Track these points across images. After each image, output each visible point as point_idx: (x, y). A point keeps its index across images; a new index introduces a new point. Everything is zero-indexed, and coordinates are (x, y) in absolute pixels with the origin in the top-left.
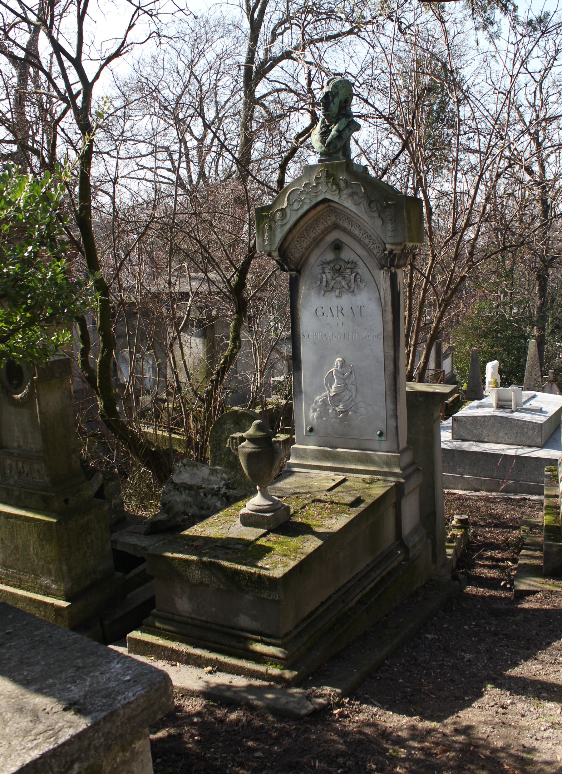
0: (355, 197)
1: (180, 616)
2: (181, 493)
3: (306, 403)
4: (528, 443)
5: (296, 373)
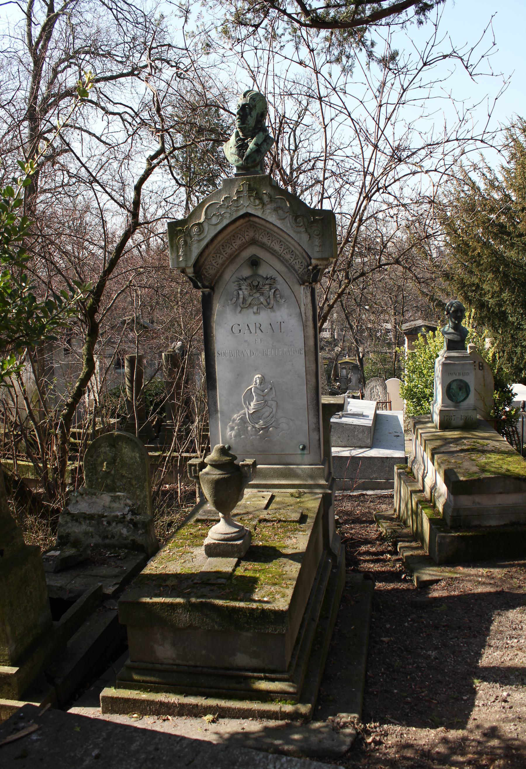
0: (280, 212)
1: (162, 664)
2: (80, 523)
3: (222, 422)
4: (358, 445)
5: (210, 392)
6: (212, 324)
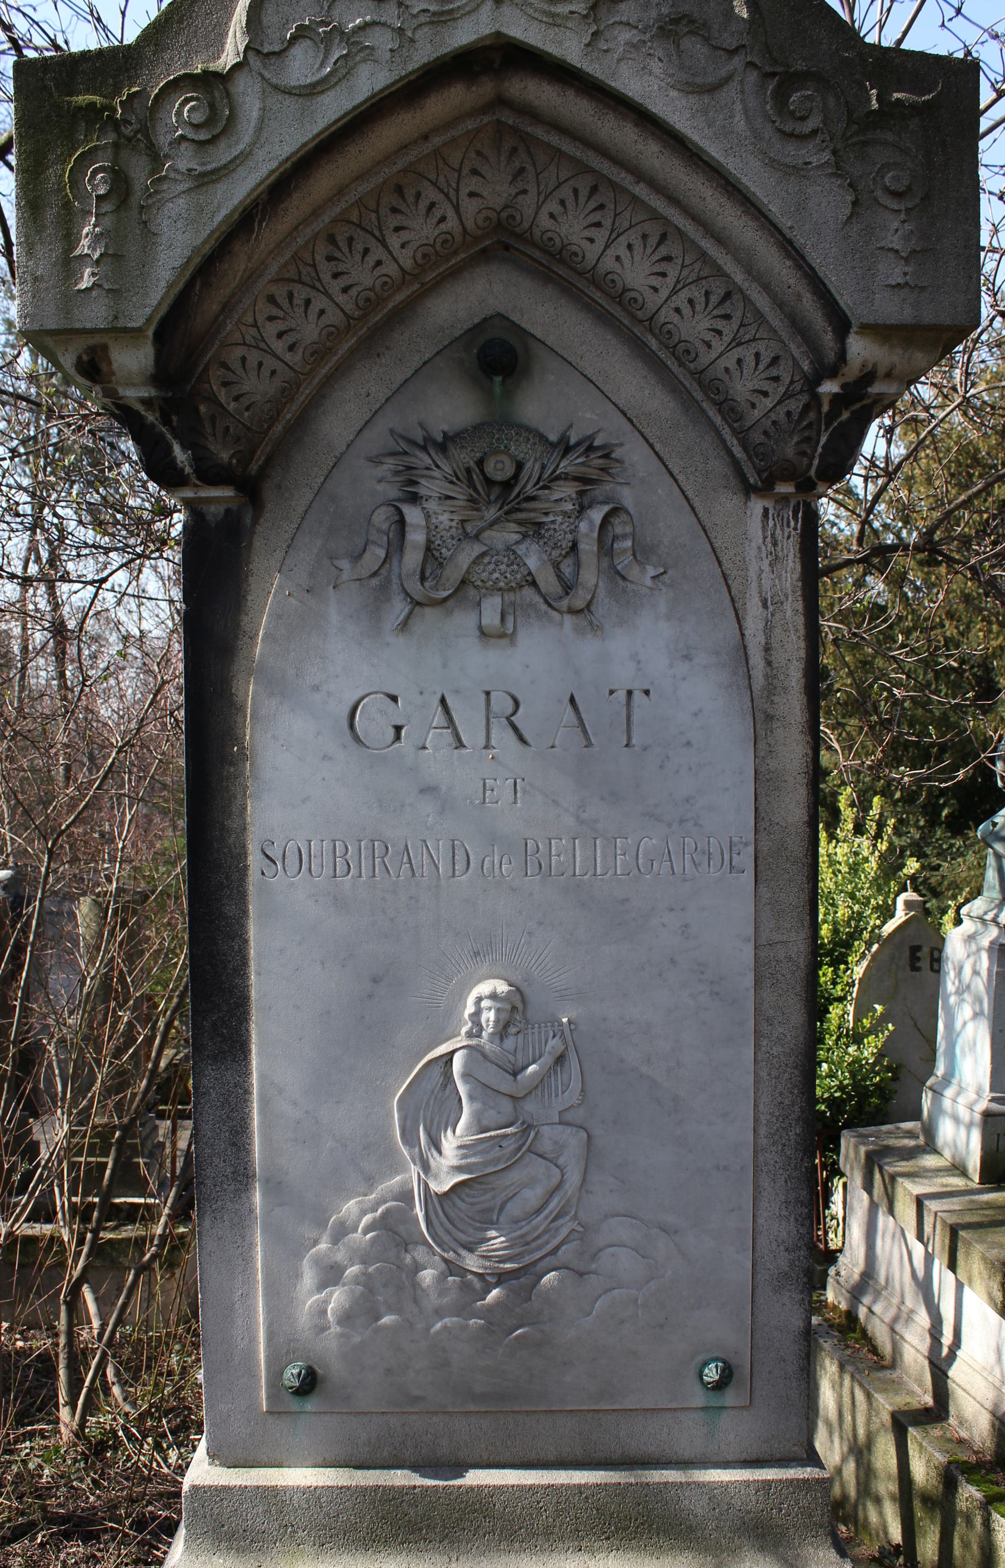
0: (694, 47)
3: (275, 1235)
6: (237, 686)
